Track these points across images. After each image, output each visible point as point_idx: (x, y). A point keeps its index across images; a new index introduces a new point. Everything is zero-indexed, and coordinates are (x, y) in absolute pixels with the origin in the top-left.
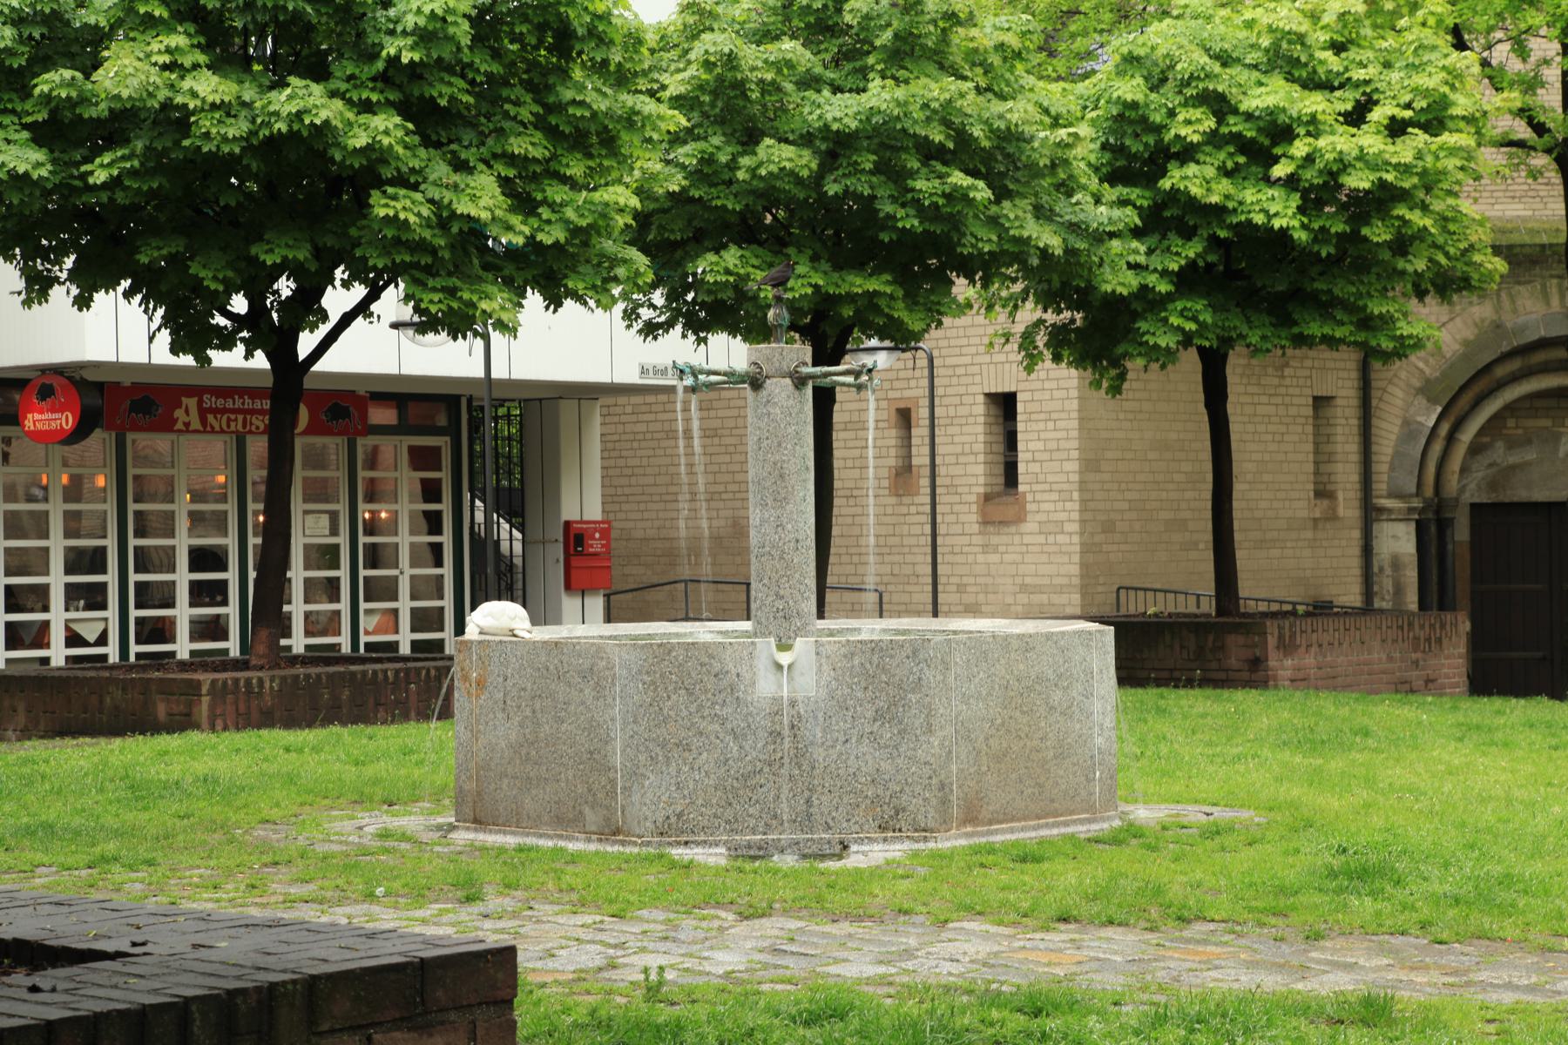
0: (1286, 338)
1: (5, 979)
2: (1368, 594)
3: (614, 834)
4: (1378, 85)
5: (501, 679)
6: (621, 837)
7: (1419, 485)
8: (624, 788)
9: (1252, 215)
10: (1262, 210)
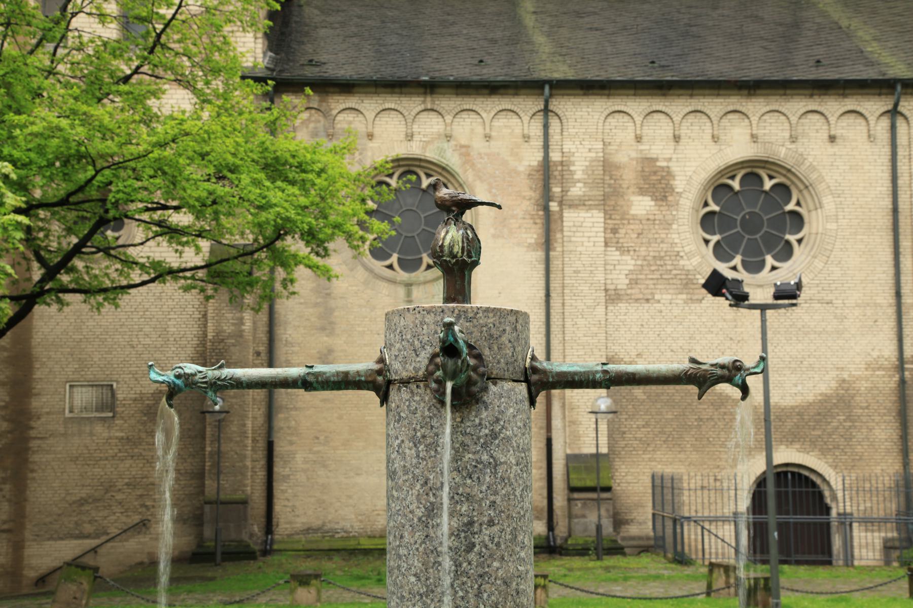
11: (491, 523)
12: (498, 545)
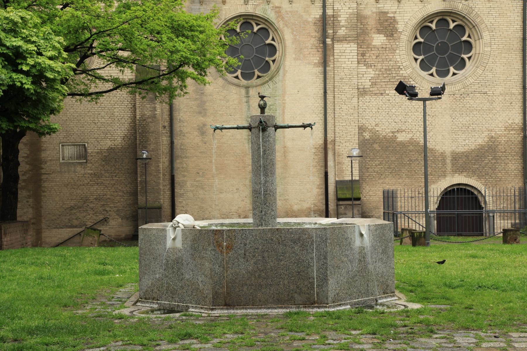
0: (12, 127)
2: (515, 209)
3: (313, 304)
4: (40, 44)
5: (242, 245)
6: (316, 305)
8: (318, 286)
9: (16, 83)
10: (19, 81)
11: (268, 150)
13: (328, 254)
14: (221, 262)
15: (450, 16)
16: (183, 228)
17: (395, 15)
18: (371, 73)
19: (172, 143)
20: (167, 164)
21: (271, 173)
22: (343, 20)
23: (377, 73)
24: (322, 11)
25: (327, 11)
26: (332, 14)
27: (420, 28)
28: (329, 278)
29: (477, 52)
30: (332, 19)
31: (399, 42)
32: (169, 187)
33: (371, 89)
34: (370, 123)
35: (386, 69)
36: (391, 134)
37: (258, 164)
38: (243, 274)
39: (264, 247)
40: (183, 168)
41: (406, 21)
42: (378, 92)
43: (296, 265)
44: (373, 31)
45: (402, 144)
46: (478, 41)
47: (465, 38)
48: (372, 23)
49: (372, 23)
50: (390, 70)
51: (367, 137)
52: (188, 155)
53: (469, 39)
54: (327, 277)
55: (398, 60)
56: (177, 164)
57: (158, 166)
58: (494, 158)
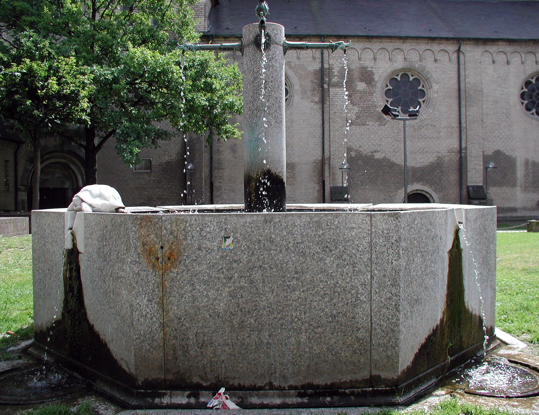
1: (538, 76)
7: (28, 183)
11: (272, 82)
12: (274, 88)
13: (401, 274)
14: (154, 291)
15: (409, 71)
16: (91, 212)
17: (373, 70)
18: (356, 109)
19: (211, 158)
20: (208, 173)
21: (276, 122)
22: (336, 71)
23: (360, 109)
24: (321, 65)
25: (324, 65)
26: (328, 67)
27: (389, 79)
28: (401, 327)
29: (429, 97)
30: (328, 71)
31: (375, 88)
32: (209, 190)
33: (356, 121)
34: (355, 145)
35: (366, 107)
36: (370, 154)
37: (253, 105)
38: (205, 319)
39: (253, 259)
40: (219, 176)
41: (380, 73)
42: (361, 123)
43: (327, 299)
44: (357, 80)
45: (379, 161)
46: (429, 90)
47: (420, 88)
48: (356, 74)
49: (356, 74)
50: (369, 108)
51: (353, 155)
52: (223, 167)
53: (423, 88)
54: (397, 325)
55: (375, 100)
56: (215, 173)
57: (201, 175)
58: (441, 172)
